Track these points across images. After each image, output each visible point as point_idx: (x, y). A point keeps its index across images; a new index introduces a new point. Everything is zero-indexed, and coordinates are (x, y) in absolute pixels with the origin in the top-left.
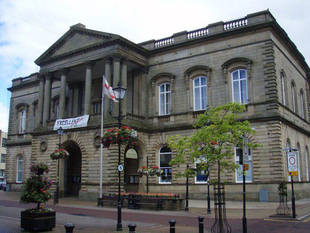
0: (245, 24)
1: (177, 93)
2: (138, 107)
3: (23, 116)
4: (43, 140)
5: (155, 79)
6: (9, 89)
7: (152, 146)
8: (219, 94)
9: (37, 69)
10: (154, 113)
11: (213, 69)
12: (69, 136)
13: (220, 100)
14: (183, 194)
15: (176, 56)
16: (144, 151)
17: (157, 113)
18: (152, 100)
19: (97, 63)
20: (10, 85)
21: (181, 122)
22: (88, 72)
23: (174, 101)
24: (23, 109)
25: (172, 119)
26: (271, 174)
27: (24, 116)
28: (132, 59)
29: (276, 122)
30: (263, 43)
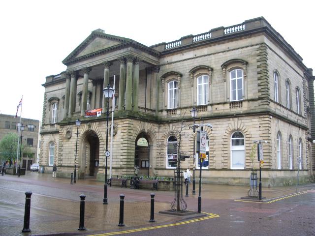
0: (243, 29)
1: (183, 90)
2: (150, 102)
3: (55, 109)
4: (68, 130)
5: (165, 76)
6: (43, 85)
7: (161, 136)
9: (64, 68)
12: (90, 126)
13: (219, 96)
14: (191, 177)
15: (183, 56)
16: (154, 140)
17: (166, 106)
18: (162, 95)
19: (114, 63)
20: (44, 82)
22: (106, 70)
23: (180, 96)
24: (55, 103)
25: (178, 112)
27: (56, 109)
28: (144, 59)
29: (267, 116)
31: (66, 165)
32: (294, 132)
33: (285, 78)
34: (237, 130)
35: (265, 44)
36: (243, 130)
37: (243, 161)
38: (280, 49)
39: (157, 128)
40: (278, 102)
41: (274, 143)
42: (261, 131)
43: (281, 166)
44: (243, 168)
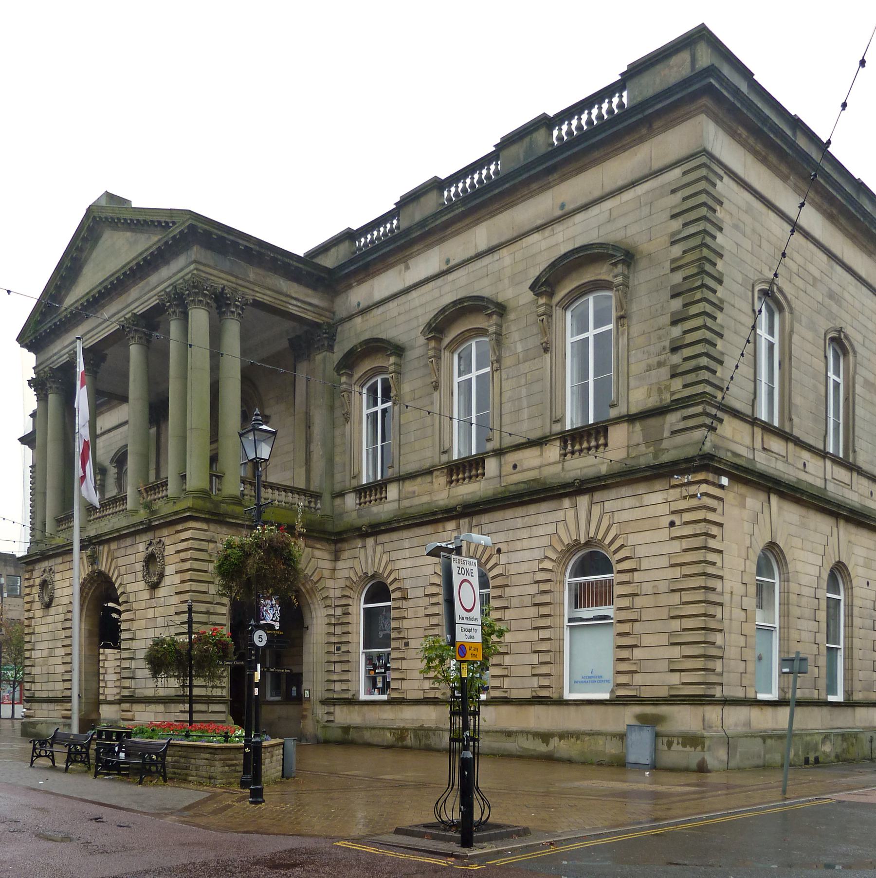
5: (349, 361)
6: (24, 440)
8: (524, 392)
10: (347, 478)
11: (511, 305)
13: (525, 414)
21: (416, 501)
25: (392, 492)
26: (672, 671)
29: (701, 476)
30: (677, 172)
31: (44, 695)
32: (858, 550)
33: (823, 325)
34: (587, 544)
35: (712, 157)
36: (607, 542)
37: (605, 666)
38: (856, 248)
39: (326, 555)
40: (776, 423)
41: (739, 589)
42: (676, 543)
43: (782, 689)
44: (606, 696)
